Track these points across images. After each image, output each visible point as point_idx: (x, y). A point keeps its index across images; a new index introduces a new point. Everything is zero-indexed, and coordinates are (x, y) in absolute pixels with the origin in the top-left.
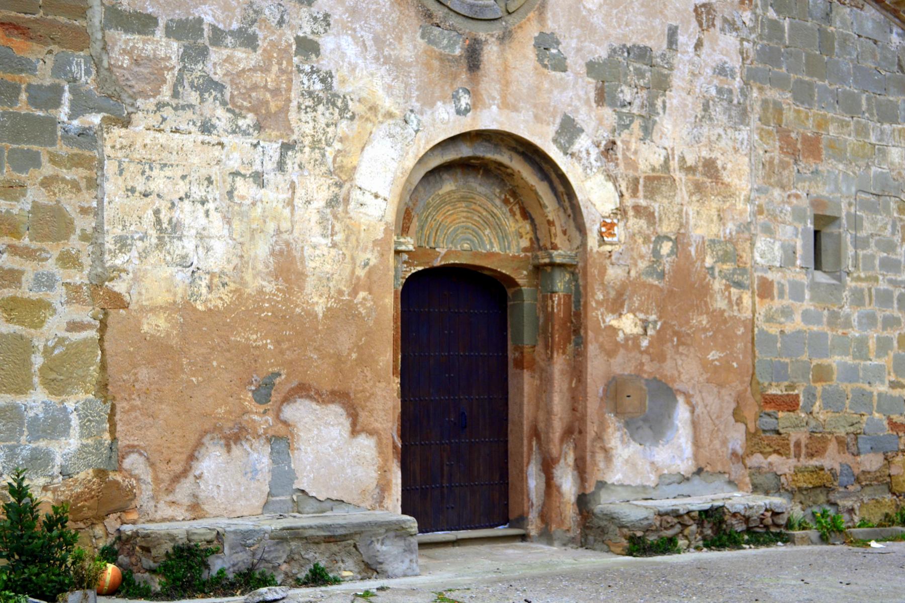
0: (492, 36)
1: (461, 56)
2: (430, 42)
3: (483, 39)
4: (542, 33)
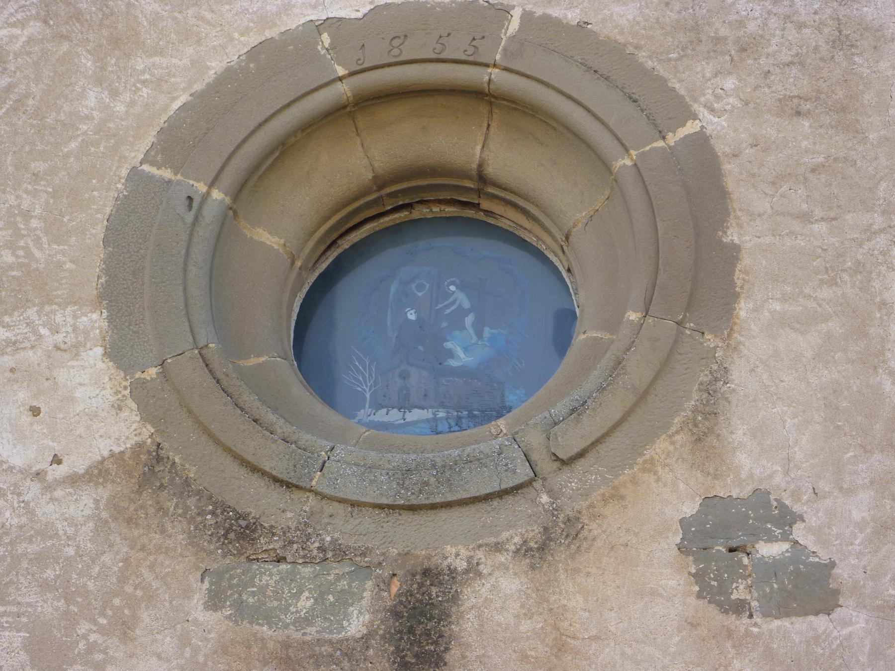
0: (498, 547)
1: (365, 640)
2: (241, 612)
3: (461, 565)
4: (709, 502)
